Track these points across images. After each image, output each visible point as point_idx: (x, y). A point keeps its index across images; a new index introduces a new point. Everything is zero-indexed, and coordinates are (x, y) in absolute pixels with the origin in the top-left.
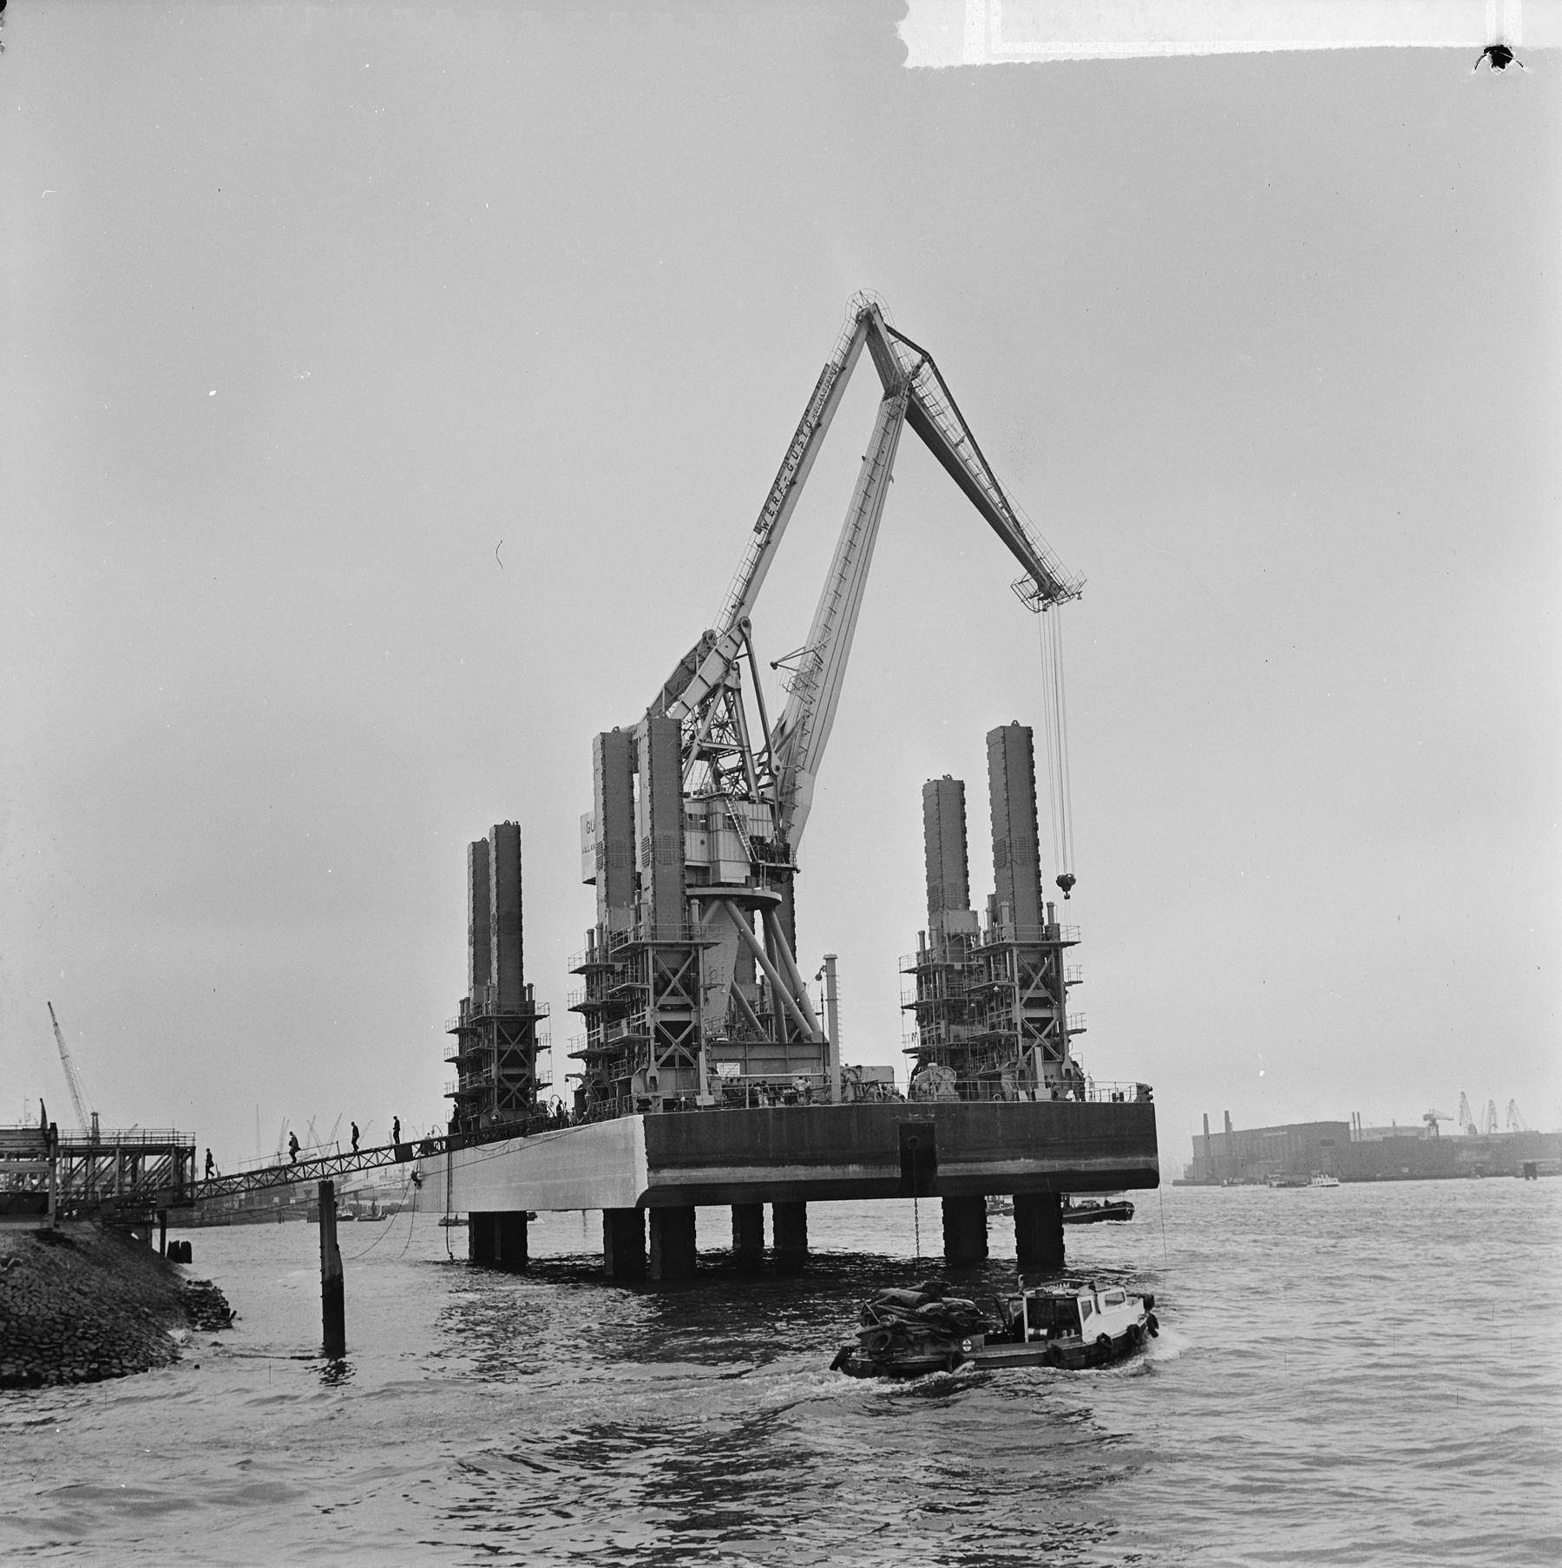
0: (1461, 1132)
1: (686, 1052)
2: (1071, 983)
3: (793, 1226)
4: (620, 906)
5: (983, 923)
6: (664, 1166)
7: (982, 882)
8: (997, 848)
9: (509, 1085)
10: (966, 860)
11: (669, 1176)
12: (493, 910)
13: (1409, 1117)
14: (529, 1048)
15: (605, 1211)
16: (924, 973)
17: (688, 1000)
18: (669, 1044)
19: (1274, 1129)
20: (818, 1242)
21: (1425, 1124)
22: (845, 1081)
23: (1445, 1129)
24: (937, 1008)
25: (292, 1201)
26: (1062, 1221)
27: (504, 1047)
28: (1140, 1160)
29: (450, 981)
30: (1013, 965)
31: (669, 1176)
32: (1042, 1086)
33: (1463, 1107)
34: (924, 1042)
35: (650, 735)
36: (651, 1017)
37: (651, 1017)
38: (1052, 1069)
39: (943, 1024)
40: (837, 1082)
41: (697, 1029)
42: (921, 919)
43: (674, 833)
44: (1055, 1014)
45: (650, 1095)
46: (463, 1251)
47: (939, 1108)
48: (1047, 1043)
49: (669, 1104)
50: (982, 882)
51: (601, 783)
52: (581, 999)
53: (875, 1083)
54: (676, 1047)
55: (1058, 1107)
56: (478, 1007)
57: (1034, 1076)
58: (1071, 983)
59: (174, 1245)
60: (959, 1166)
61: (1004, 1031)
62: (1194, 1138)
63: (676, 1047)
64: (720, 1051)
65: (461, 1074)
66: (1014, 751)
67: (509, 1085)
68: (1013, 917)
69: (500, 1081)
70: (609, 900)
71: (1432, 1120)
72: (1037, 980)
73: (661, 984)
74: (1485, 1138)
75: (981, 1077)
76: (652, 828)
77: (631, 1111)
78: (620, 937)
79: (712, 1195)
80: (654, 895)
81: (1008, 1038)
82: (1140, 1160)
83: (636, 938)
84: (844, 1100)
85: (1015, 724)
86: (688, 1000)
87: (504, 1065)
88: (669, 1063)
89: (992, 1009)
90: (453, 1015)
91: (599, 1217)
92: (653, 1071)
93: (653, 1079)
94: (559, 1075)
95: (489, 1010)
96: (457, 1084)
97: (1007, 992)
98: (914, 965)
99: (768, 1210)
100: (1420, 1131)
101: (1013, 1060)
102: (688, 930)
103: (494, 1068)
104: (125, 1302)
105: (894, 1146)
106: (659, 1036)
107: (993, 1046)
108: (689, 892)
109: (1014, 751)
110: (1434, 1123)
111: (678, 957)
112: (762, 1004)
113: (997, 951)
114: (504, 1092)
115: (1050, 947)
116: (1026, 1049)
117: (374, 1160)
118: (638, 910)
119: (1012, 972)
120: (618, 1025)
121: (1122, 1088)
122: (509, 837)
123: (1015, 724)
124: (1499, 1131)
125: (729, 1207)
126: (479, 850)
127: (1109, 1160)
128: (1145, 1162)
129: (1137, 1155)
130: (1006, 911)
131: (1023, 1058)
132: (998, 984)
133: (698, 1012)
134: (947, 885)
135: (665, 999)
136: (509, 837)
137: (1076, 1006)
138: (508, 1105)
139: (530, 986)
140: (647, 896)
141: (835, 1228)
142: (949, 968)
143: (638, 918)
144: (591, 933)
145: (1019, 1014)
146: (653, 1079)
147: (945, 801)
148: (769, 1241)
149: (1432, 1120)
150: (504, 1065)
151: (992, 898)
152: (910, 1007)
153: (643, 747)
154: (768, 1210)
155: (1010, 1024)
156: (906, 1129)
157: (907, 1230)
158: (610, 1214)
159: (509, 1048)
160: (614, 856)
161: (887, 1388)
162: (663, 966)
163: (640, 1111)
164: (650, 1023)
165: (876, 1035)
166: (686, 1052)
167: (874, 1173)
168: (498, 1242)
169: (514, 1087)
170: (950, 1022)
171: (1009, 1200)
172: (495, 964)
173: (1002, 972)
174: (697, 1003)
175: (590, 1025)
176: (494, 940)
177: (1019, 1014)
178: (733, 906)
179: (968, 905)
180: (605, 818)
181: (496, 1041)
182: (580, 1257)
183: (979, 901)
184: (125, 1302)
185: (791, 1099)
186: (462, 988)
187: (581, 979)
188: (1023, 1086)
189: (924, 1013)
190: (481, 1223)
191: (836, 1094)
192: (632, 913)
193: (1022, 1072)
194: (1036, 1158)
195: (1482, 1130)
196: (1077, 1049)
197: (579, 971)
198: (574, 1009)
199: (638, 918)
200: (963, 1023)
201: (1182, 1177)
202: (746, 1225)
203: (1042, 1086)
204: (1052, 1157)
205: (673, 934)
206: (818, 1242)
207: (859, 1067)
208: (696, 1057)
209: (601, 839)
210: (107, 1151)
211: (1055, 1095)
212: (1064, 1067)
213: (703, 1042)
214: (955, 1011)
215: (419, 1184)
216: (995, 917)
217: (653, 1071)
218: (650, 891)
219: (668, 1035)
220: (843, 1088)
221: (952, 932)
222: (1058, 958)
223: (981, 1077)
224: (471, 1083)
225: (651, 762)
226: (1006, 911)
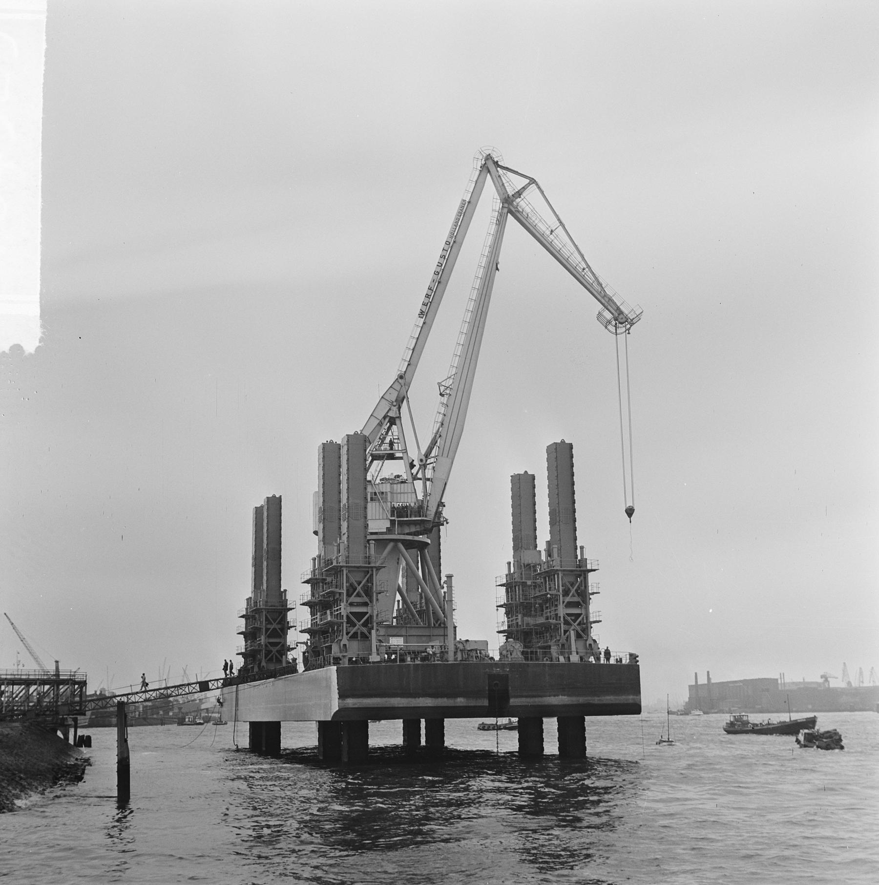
0: (843, 685)
1: (365, 630)
2: (593, 593)
3: (437, 732)
4: (331, 544)
5: (543, 558)
7: (544, 534)
8: (551, 514)
9: (272, 648)
10: (535, 521)
11: (351, 702)
12: (265, 546)
13: (814, 677)
14: (284, 627)
16: (510, 586)
17: (366, 599)
18: (355, 625)
19: (736, 682)
20: (450, 742)
21: (821, 681)
22: (457, 649)
23: (833, 684)
24: (517, 607)
25: (171, 714)
27: (269, 626)
29: (241, 590)
30: (559, 582)
31: (351, 702)
32: (574, 654)
33: (844, 671)
34: (509, 627)
36: (344, 609)
37: (344, 609)
38: (581, 643)
39: (520, 616)
40: (451, 649)
41: (371, 617)
44: (583, 612)
46: (245, 742)
48: (578, 628)
50: (544, 534)
52: (308, 597)
54: (359, 627)
58: (593, 593)
59: (82, 737)
60: (524, 699)
63: (359, 627)
64: (391, 630)
65: (246, 642)
66: (562, 458)
67: (272, 648)
68: (559, 555)
69: (266, 646)
71: (825, 678)
72: (573, 591)
73: (351, 590)
74: (856, 689)
75: (540, 648)
77: (330, 664)
78: (329, 562)
79: (550, 711)
81: (555, 625)
82: (630, 698)
84: (456, 660)
85: (563, 442)
86: (366, 599)
87: (269, 637)
88: (354, 636)
89: (547, 608)
91: (314, 726)
92: (345, 641)
93: (345, 645)
94: (297, 640)
95: (261, 605)
96: (243, 647)
98: (504, 581)
99: (423, 721)
102: (368, 559)
103: (263, 637)
105: (487, 688)
106: (349, 621)
107: (547, 630)
109: (562, 458)
110: (826, 680)
111: (363, 574)
112: (421, 603)
113: (550, 574)
114: (268, 652)
115: (581, 571)
116: (565, 632)
117: (191, 689)
121: (622, 655)
122: (275, 505)
123: (563, 442)
126: (258, 511)
127: (612, 697)
128: (633, 699)
130: (555, 550)
131: (564, 637)
132: (550, 593)
134: (523, 537)
135: (353, 599)
136: (275, 505)
137: (595, 607)
139: (285, 591)
140: (345, 538)
142: (524, 584)
143: (339, 551)
144: (314, 559)
145: (562, 611)
146: (345, 645)
147: (523, 486)
148: (423, 742)
149: (825, 678)
150: (269, 637)
151: (548, 543)
152: (501, 606)
153: (344, 451)
154: (423, 721)
155: (557, 617)
156: (491, 677)
158: (254, 726)
161: (780, 786)
162: (353, 580)
163: (334, 664)
165: (480, 620)
166: (365, 630)
167: (472, 703)
169: (274, 649)
170: (524, 615)
171: (515, 720)
172: (265, 578)
173: (552, 586)
174: (371, 601)
175: (313, 614)
176: (265, 563)
177: (562, 611)
178: (401, 546)
181: (265, 621)
183: (542, 546)
186: (248, 591)
187: (308, 587)
188: (562, 653)
189: (510, 609)
191: (451, 657)
192: (336, 548)
193: (563, 645)
194: (568, 695)
195: (855, 684)
196: (596, 632)
197: (307, 582)
198: (303, 604)
200: (530, 616)
202: (411, 731)
203: (574, 654)
204: (578, 695)
206: (450, 742)
207: (467, 641)
208: (370, 633)
211: (581, 658)
212: (588, 643)
213: (375, 624)
215: (221, 704)
216: (549, 554)
217: (345, 641)
218: (346, 536)
219: (355, 620)
220: (455, 653)
221: (526, 563)
223: (540, 648)
224: (251, 646)
226: (555, 550)
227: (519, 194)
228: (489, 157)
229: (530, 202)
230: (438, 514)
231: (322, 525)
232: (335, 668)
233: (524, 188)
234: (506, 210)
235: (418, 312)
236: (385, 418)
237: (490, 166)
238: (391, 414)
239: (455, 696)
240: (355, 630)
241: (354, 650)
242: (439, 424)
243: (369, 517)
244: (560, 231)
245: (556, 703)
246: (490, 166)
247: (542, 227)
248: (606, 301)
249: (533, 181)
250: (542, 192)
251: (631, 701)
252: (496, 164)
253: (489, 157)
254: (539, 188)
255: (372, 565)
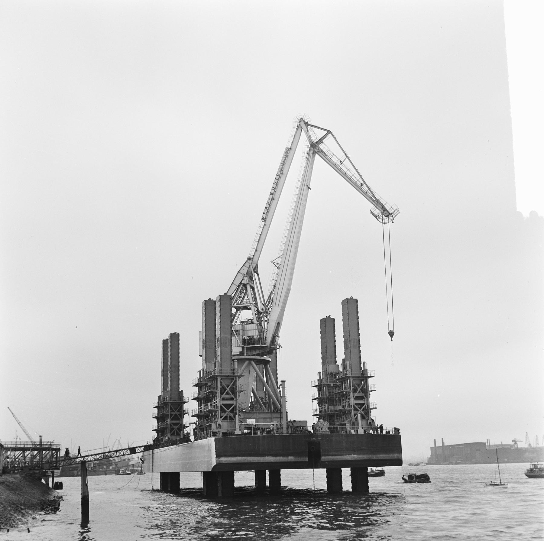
0: (526, 446)
1: (231, 415)
2: (371, 391)
3: (276, 477)
4: (210, 362)
5: (341, 369)
6: (222, 456)
9: (174, 427)
11: (223, 459)
14: (182, 413)
15: (161, 473)
16: (320, 387)
17: (232, 396)
18: (225, 412)
21: (513, 443)
22: (288, 426)
23: (520, 445)
25: (111, 468)
26: (367, 475)
27: (172, 413)
28: (396, 455)
29: (155, 390)
30: (350, 384)
31: (223, 459)
32: (361, 428)
34: (320, 412)
35: (220, 301)
36: (219, 402)
37: (219, 402)
38: (364, 422)
40: (285, 426)
41: (235, 406)
42: (319, 368)
43: (229, 336)
45: (217, 430)
46: (158, 486)
47: (322, 436)
48: (363, 413)
49: (224, 434)
51: (204, 318)
52: (196, 395)
53: (300, 427)
55: (367, 435)
56: (164, 399)
57: (358, 424)
58: (371, 391)
59: (57, 483)
60: (330, 457)
61: (348, 408)
62: (431, 448)
65: (158, 423)
66: (350, 306)
67: (174, 427)
68: (351, 367)
69: (170, 425)
70: (206, 360)
72: (359, 389)
73: (223, 391)
75: (339, 425)
76: (221, 334)
78: (209, 373)
80: (221, 358)
81: (349, 411)
82: (396, 455)
83: (214, 373)
84: (288, 433)
85: (352, 298)
86: (232, 396)
87: (172, 419)
88: (225, 419)
89: (343, 400)
90: (155, 401)
92: (219, 421)
93: (219, 424)
95: (167, 400)
96: (157, 426)
97: (348, 394)
98: (317, 384)
99: (267, 471)
100: (511, 446)
101: (350, 419)
102: (233, 371)
103: (168, 420)
104: (14, 504)
106: (222, 409)
108: (233, 358)
109: (350, 306)
110: (516, 443)
111: (230, 381)
112: (265, 398)
114: (172, 429)
116: (355, 415)
117: (118, 453)
118: (215, 363)
119: (350, 387)
120: (208, 405)
121: (389, 429)
122: (175, 337)
123: (352, 298)
124: (539, 446)
125: (349, 469)
126: (165, 342)
127: (384, 455)
128: (397, 456)
129: (395, 453)
130: (348, 365)
131: (354, 418)
133: (236, 400)
134: (328, 355)
136: (175, 337)
137: (373, 399)
138: (173, 434)
139: (182, 391)
140: (219, 358)
141: (293, 479)
143: (215, 366)
144: (200, 372)
147: (327, 324)
148: (268, 483)
150: (172, 419)
151: (343, 360)
152: (315, 399)
154: (267, 471)
155: (349, 405)
157: (315, 479)
159: (174, 413)
160: (209, 344)
162: (224, 384)
163: (213, 436)
164: (218, 404)
166: (231, 415)
167: (298, 459)
168: (170, 483)
169: (176, 427)
170: (329, 405)
173: (346, 387)
174: (235, 397)
176: (170, 374)
177: (353, 402)
178: (253, 363)
179: (336, 362)
180: (206, 331)
181: (169, 409)
182: (250, 486)
183: (339, 362)
184: (14, 504)
185: (268, 432)
188: (353, 428)
189: (320, 401)
190: (164, 476)
193: (353, 423)
194: (357, 454)
196: (374, 415)
197: (196, 385)
199: (215, 366)
200: (333, 405)
201: (427, 462)
202: (260, 478)
204: (364, 454)
205: (227, 372)
207: (295, 421)
208: (235, 417)
209: (204, 338)
210: (46, 449)
211: (365, 431)
214: (331, 401)
215: (143, 462)
216: (344, 366)
218: (220, 357)
220: (287, 429)
221: (330, 372)
222: (367, 382)
223: (339, 425)
225: (220, 311)
226: (348, 365)
227: (321, 141)
228: (301, 120)
229: (328, 145)
230: (273, 341)
231: (204, 350)
232: (214, 438)
233: (324, 137)
234: (312, 152)
235: (261, 218)
236: (241, 283)
237: (303, 124)
238: (243, 282)
239: (288, 455)
240: (225, 415)
241: (225, 426)
242: (273, 287)
243: (234, 345)
244: (347, 162)
245: (350, 459)
246: (303, 124)
247: (334, 159)
248: (377, 203)
249: (329, 132)
250: (335, 138)
251: (396, 458)
252: (307, 124)
253: (301, 120)
254: (333, 136)
255: (236, 375)
